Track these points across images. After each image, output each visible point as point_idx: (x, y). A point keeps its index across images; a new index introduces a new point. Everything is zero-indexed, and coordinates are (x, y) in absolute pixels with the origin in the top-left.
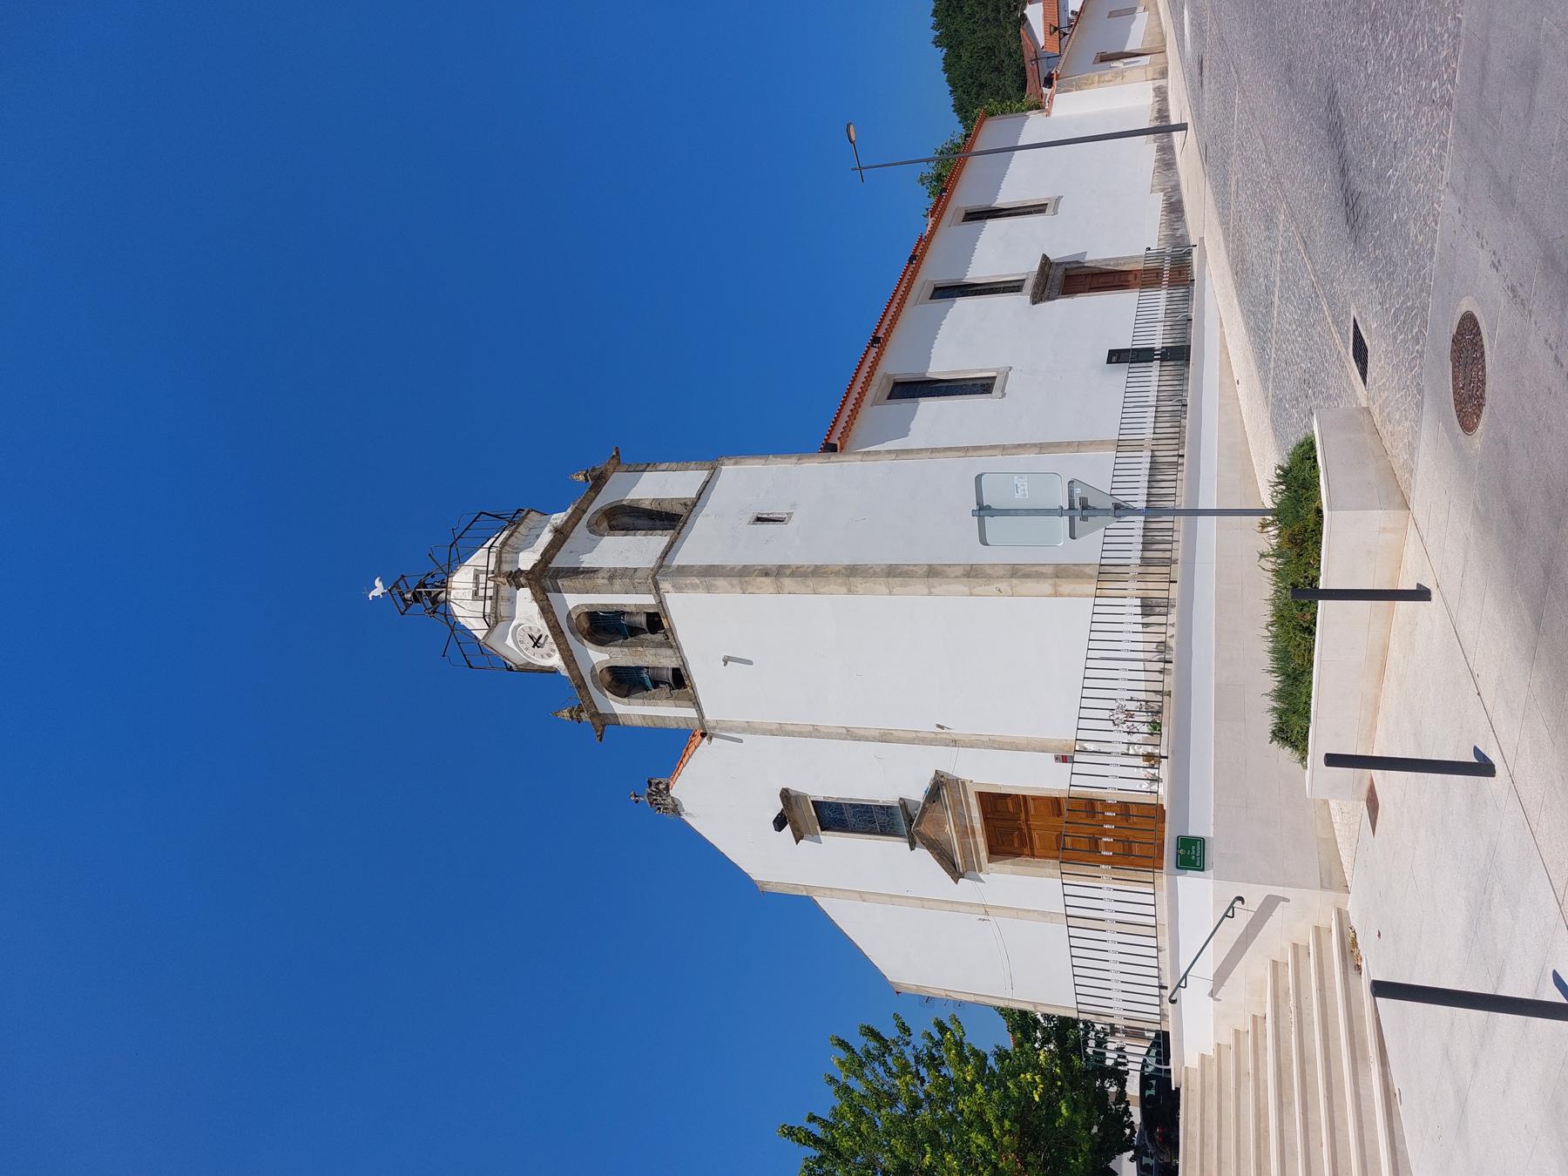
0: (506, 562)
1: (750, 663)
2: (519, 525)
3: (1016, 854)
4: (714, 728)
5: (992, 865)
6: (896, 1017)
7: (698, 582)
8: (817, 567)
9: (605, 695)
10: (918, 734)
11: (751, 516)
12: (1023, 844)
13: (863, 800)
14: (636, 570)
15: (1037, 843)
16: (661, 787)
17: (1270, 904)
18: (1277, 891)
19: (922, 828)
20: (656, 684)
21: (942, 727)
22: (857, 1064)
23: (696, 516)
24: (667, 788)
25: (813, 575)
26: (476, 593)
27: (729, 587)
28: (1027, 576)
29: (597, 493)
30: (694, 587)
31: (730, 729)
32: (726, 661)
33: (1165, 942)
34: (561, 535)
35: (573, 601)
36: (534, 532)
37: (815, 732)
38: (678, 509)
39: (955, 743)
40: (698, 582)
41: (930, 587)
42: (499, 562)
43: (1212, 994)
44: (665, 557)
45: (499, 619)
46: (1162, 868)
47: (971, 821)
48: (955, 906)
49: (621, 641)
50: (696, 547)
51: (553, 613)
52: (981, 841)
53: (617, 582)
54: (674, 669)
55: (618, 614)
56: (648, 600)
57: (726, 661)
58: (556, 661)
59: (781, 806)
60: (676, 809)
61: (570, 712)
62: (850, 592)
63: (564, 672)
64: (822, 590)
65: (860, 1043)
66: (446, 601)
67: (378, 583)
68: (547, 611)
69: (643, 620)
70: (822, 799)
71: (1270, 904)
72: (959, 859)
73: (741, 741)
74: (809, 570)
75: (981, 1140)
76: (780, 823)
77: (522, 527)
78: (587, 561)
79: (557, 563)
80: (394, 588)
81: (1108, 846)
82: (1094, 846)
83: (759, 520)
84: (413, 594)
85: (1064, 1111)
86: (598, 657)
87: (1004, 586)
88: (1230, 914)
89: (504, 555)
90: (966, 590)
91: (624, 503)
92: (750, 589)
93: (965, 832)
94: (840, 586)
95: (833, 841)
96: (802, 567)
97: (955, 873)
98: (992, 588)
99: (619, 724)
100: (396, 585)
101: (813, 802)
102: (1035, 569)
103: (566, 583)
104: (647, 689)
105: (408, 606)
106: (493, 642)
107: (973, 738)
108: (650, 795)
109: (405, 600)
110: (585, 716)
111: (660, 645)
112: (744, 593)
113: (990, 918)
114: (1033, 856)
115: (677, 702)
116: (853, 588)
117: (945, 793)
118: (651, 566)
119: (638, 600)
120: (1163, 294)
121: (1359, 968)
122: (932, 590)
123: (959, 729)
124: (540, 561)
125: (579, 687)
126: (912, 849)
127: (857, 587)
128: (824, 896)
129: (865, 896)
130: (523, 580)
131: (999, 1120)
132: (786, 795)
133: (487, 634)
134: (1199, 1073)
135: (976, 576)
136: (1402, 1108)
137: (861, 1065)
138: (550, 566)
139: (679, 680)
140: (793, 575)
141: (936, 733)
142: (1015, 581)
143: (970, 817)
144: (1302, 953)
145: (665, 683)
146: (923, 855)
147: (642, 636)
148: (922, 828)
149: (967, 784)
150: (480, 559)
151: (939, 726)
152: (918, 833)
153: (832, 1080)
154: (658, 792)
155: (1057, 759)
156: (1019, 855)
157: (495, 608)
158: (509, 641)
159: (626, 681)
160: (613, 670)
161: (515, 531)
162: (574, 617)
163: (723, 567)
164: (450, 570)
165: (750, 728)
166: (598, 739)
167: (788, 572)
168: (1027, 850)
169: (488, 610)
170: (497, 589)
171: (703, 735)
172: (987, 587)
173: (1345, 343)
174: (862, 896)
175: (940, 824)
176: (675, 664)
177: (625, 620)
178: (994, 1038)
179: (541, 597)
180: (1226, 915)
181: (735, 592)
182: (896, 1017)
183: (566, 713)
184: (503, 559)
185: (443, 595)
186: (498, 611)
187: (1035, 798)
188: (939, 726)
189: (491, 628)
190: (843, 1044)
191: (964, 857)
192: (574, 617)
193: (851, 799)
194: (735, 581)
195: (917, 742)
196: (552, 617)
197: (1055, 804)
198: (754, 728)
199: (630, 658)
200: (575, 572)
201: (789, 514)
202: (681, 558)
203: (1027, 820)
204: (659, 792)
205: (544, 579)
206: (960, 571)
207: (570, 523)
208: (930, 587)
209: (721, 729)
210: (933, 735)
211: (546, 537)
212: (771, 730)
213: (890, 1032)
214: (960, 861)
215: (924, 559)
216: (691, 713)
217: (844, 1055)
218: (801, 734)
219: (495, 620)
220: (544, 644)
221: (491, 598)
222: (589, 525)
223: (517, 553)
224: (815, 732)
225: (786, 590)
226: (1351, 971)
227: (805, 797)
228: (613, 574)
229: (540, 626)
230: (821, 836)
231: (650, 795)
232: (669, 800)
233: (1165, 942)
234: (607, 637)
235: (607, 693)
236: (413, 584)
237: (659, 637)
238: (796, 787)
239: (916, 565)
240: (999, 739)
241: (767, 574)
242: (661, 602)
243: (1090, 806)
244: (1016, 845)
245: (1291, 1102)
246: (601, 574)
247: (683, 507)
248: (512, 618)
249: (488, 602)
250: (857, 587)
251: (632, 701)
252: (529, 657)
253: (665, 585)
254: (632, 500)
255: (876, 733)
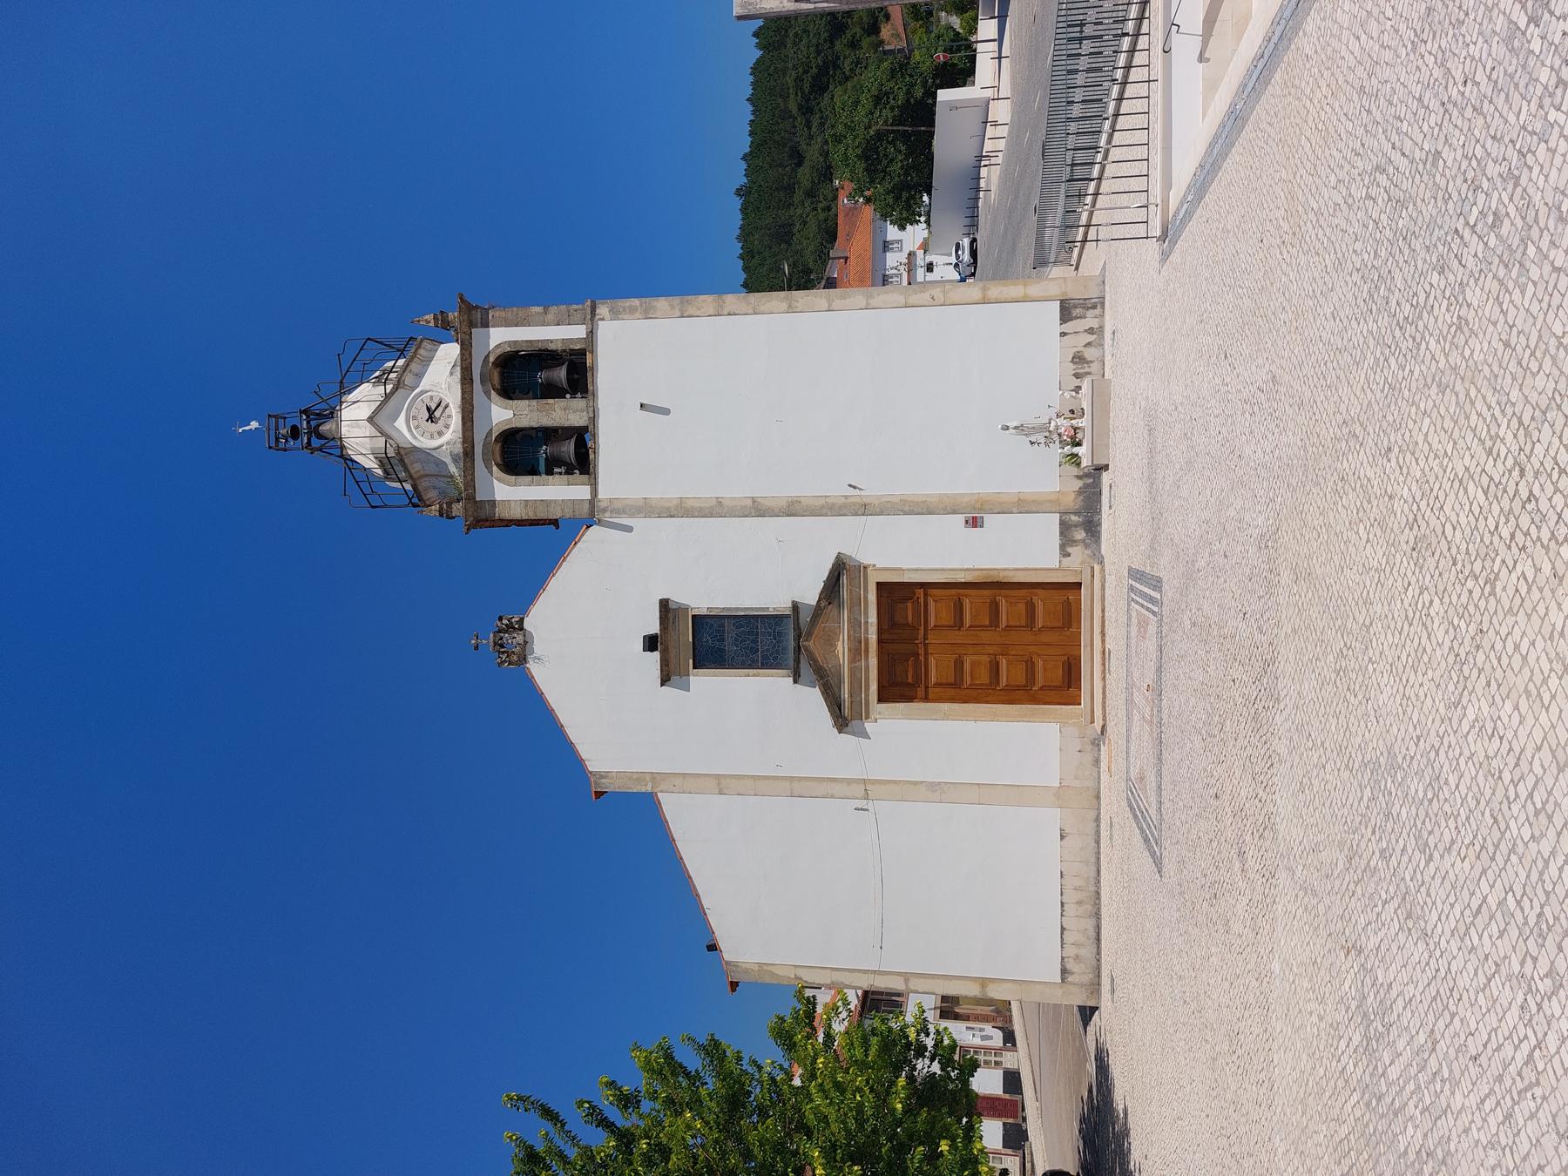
0: (424, 348)
1: (666, 412)
3: (910, 699)
10: (827, 500)
13: (752, 609)
19: (811, 644)
21: (855, 487)
31: (619, 512)
37: (717, 510)
45: (401, 385)
70: (705, 612)
73: (629, 529)
76: (651, 643)
92: (691, 311)
113: (870, 805)
117: (845, 581)
123: (873, 490)
127: (798, 302)
133: (380, 405)
141: (846, 497)
143: (867, 623)
148: (811, 644)
152: (806, 649)
155: (967, 522)
164: (345, 388)
166: (464, 529)
172: (922, 294)
173: (1211, 87)
184: (422, 346)
186: (403, 378)
191: (851, 695)
193: (738, 609)
195: (824, 511)
196: (468, 357)
197: (956, 590)
198: (652, 507)
214: (846, 696)
220: (439, 418)
224: (717, 510)
227: (686, 609)
235: (495, 468)
238: (679, 597)
242: (592, 332)
250: (798, 302)
252: (415, 438)
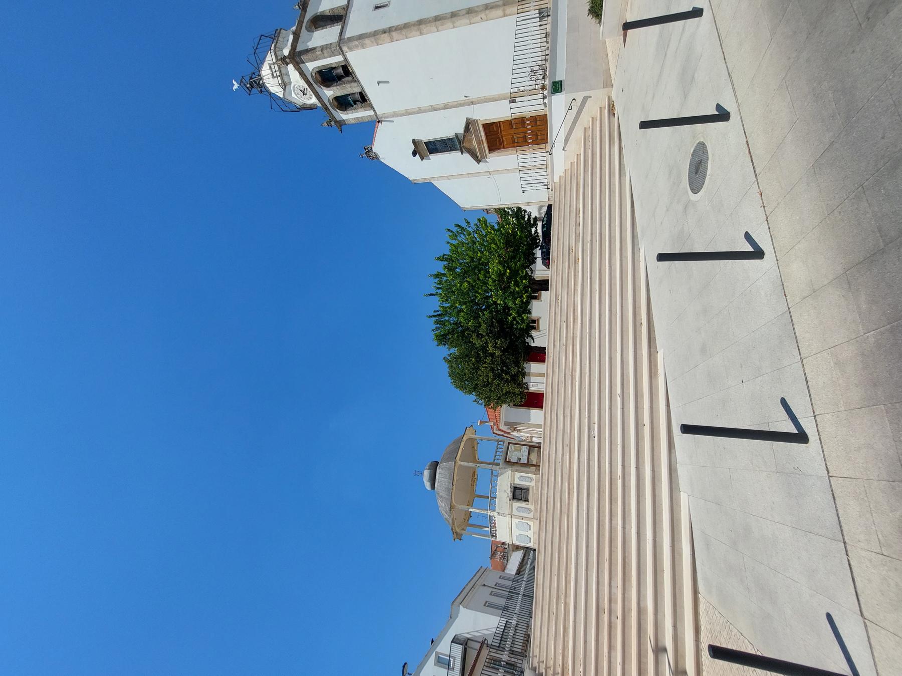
2: (278, 37)
4: (382, 117)
5: (491, 154)
6: (465, 219)
7: (357, 43)
8: (405, 24)
9: (337, 111)
11: (373, 7)
12: (500, 144)
14: (331, 44)
15: (505, 143)
16: (369, 149)
17: (586, 99)
18: (586, 94)
20: (355, 102)
22: (455, 236)
23: (350, 12)
24: (371, 149)
25: (404, 28)
26: (273, 75)
27: (371, 43)
28: (492, 8)
29: (306, 12)
30: (357, 47)
31: (387, 117)
32: (379, 83)
33: (549, 171)
34: (297, 35)
35: (311, 66)
36: (286, 39)
37: (420, 111)
38: (342, 12)
39: (472, 103)
40: (357, 43)
41: (453, 23)
42: (276, 56)
43: (563, 149)
44: (341, 35)
46: (548, 143)
47: (481, 138)
48: (480, 174)
49: (335, 84)
50: (355, 25)
51: (305, 75)
52: (485, 145)
53: (325, 51)
54: (359, 92)
55: (331, 69)
56: (339, 58)
57: (379, 83)
58: (314, 100)
59: (413, 147)
60: (377, 157)
61: (327, 123)
62: (421, 34)
63: (319, 105)
64: (409, 36)
65: (455, 229)
66: (263, 83)
67: (234, 82)
68: (302, 74)
69: (340, 71)
70: (427, 141)
71: (586, 99)
72: (479, 155)
74: (402, 26)
75: (494, 246)
76: (414, 154)
77: (280, 38)
78: (310, 45)
79: (299, 49)
80: (241, 83)
81: (528, 124)
82: (525, 138)
83: (377, 8)
84: (250, 84)
85: (519, 234)
86: (329, 93)
87: (483, 15)
88: (570, 108)
89: (277, 53)
90: (468, 21)
91: (318, 14)
92: (380, 42)
93: (480, 143)
94: (417, 31)
95: (435, 158)
96: (399, 25)
97: (478, 161)
98: (478, 18)
99: (346, 124)
100: (241, 81)
101: (424, 143)
102: (495, 4)
103: (305, 57)
104: (352, 106)
105: (250, 91)
106: (287, 97)
107: (479, 99)
108: (366, 153)
109: (248, 88)
110: (332, 123)
111: (351, 82)
112: (378, 45)
114: (504, 148)
115: (365, 109)
116: (422, 32)
118: (337, 41)
119: (335, 60)
120: (564, 95)
121: (614, 114)
122: (455, 25)
123: (473, 96)
124: (291, 49)
125: (326, 110)
126: (462, 154)
128: (435, 180)
129: (449, 177)
130: (288, 60)
131: (499, 240)
132: (414, 142)
134: (559, 184)
135: (471, 13)
136: (624, 151)
137: (456, 236)
138: (296, 51)
139: (363, 99)
140: (396, 30)
142: (487, 12)
143: (481, 136)
144: (595, 120)
145: (358, 101)
146: (467, 156)
147: (343, 80)
149: (479, 121)
150: (270, 58)
151: (465, 96)
152: (463, 147)
153: (448, 243)
154: (369, 151)
156: (499, 149)
157: (282, 79)
158: (293, 95)
159: (343, 103)
160: (337, 99)
161: (278, 40)
162: (314, 75)
163: (366, 34)
164: (259, 69)
165: (395, 115)
167: (394, 29)
168: (502, 146)
169: (280, 82)
170: (279, 67)
171: (379, 122)
174: (448, 177)
175: (471, 142)
176: (359, 90)
177: (334, 72)
178: (494, 220)
179: (297, 67)
180: (569, 109)
181: (374, 46)
182: (465, 219)
183: (325, 124)
184: (278, 55)
185: (261, 82)
187: (503, 122)
188: (465, 96)
189: (284, 90)
190: (449, 230)
191: (480, 154)
192: (314, 75)
194: (372, 39)
197: (510, 123)
199: (341, 91)
200: (307, 51)
201: (389, 2)
202: (348, 34)
203: (501, 133)
204: (369, 151)
205: (296, 58)
206: (464, 12)
207: (298, 29)
208: (453, 23)
209: (384, 117)
210: (464, 101)
211: (291, 37)
212: (403, 114)
213: (464, 225)
215: (449, 10)
216: (371, 113)
217: (451, 234)
218: (414, 113)
219: (285, 85)
221: (279, 76)
222: (306, 28)
223: (282, 50)
225: (395, 39)
226: (611, 116)
227: (421, 141)
228: (323, 48)
229: (302, 84)
230: (430, 157)
231: (366, 153)
232: (374, 154)
233: (549, 171)
234: (328, 84)
236: (247, 78)
237: (349, 78)
238: (418, 138)
239: (445, 14)
240: (488, 97)
241: (385, 32)
243: (521, 121)
244: (498, 145)
245: (588, 171)
246: (317, 50)
247: (343, 11)
248: (290, 83)
249: (279, 78)
251: (349, 112)
253: (345, 49)
254: (321, 12)
255: (442, 106)
